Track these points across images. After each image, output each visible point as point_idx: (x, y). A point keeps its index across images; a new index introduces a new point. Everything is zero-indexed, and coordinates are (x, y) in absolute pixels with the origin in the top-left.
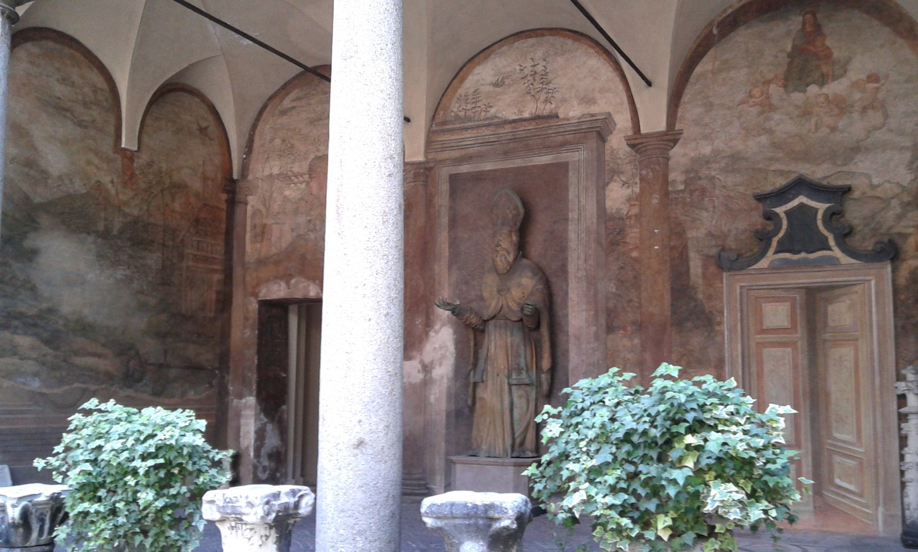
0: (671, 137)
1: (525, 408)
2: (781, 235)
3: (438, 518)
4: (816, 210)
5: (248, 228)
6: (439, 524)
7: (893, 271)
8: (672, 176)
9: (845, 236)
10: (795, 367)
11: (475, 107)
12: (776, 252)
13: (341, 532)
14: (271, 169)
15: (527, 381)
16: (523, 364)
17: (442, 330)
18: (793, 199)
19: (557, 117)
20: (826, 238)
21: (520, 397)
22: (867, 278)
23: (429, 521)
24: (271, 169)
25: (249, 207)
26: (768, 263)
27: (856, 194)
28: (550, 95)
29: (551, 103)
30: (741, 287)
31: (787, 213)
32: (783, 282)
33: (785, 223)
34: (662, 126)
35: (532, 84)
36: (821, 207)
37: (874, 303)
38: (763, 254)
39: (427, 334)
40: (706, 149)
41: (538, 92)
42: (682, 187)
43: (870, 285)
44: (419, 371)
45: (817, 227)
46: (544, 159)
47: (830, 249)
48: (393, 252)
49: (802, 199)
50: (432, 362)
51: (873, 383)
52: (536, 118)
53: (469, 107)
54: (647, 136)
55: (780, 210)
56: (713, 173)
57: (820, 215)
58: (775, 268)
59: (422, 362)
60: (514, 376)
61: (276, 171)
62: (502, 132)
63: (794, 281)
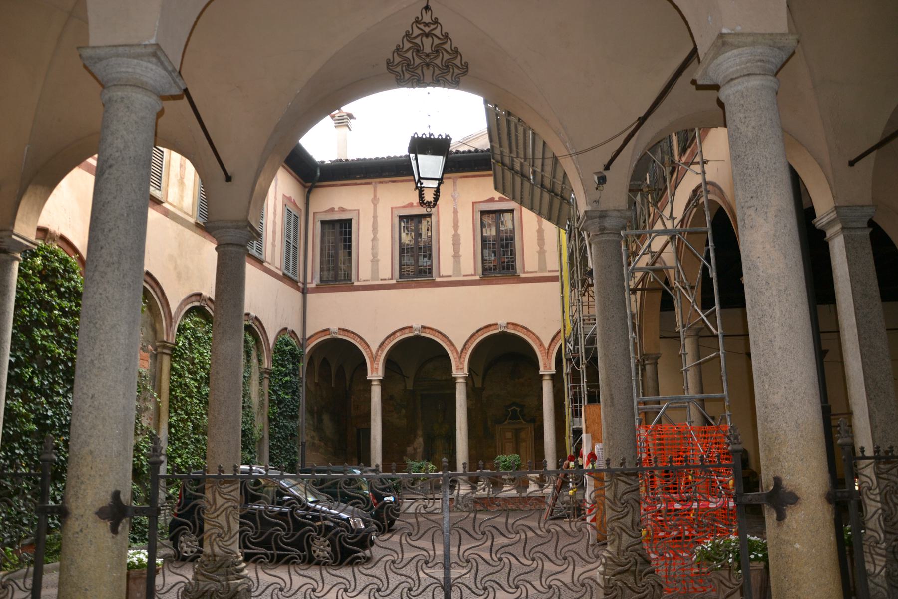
0: (483, 389)
36: (518, 409)
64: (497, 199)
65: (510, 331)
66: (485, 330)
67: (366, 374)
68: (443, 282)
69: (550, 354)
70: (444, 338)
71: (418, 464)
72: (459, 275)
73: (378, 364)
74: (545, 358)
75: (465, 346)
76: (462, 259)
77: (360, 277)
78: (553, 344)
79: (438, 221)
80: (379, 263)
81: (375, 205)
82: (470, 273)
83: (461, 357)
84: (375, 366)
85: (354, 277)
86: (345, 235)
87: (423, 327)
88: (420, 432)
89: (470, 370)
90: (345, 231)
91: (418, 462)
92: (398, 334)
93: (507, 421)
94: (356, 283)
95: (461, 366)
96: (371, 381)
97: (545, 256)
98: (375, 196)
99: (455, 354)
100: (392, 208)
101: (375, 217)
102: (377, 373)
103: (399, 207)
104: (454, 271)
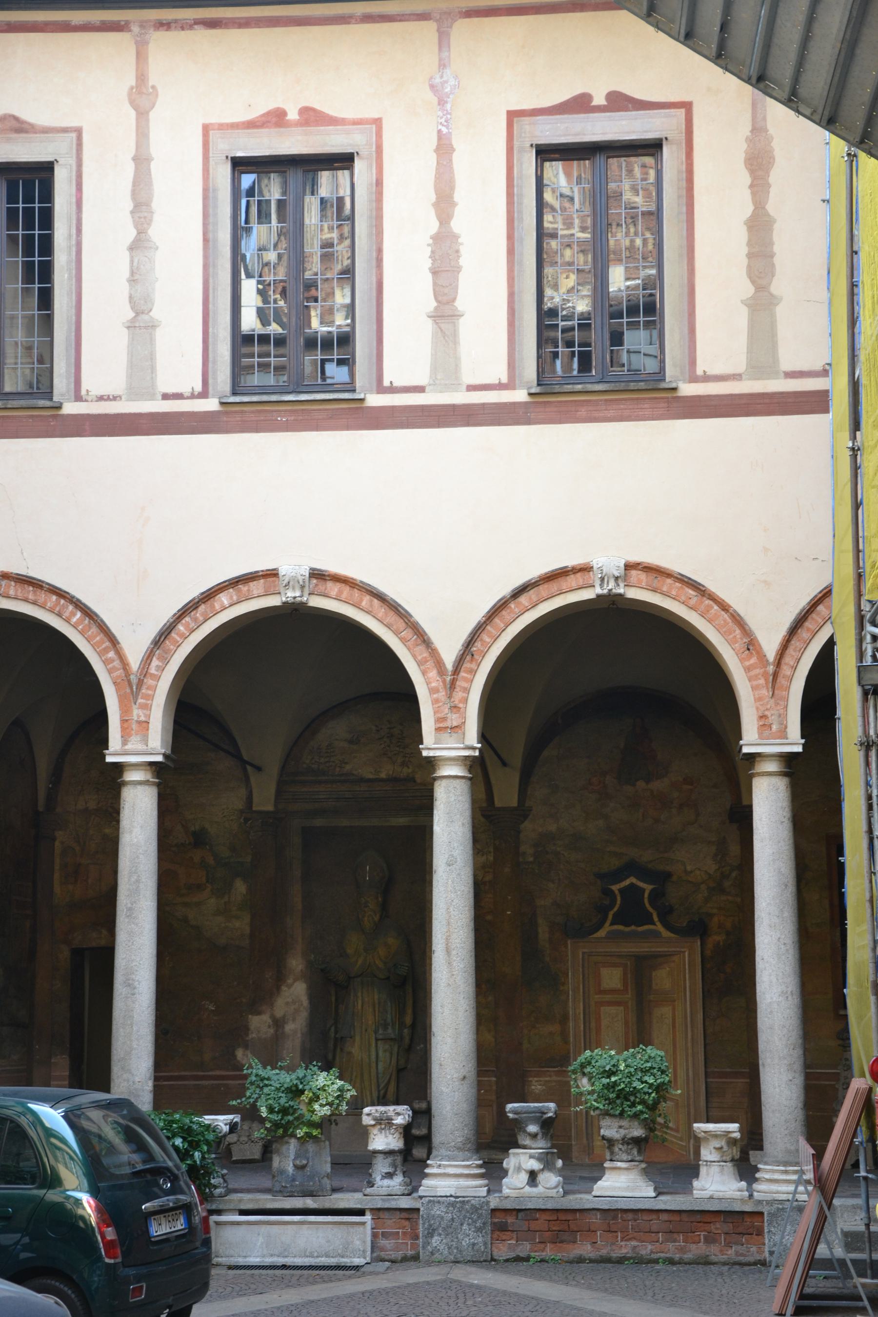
0: (522, 812)
1: (388, 1061)
2: (615, 909)
3: (515, 1114)
4: (644, 890)
5: (57, 867)
6: (516, 1116)
7: (702, 945)
8: (523, 848)
9: (665, 914)
10: (626, 1023)
11: (329, 762)
12: (612, 924)
13: (456, 1125)
14: (86, 803)
15: (392, 1036)
16: (389, 1020)
17: (295, 984)
18: (625, 879)
19: (415, 781)
20: (651, 914)
21: (385, 1051)
22: (683, 950)
23: (511, 1115)
24: (86, 803)
25: (57, 843)
26: (605, 933)
27: (674, 878)
28: (407, 759)
29: (408, 768)
30: (584, 953)
31: (620, 891)
32: (618, 950)
33: (619, 898)
34: (514, 803)
35: (389, 746)
36: (648, 888)
37: (687, 971)
38: (599, 926)
39: (278, 989)
40: (553, 827)
41: (395, 754)
42: (531, 859)
43: (684, 956)
44: (269, 1027)
45: (644, 904)
46: (402, 821)
47: (654, 924)
48: (797, 1075)
49: (632, 880)
50: (284, 1016)
51: (686, 1037)
52: (393, 780)
53: (322, 760)
54: (499, 809)
55: (615, 888)
56: (558, 849)
57: (646, 895)
58: (612, 937)
59: (273, 1017)
60: (381, 1032)
61: (92, 805)
62: (358, 789)
63: (626, 950)
64: (599, 100)
65: (633, 594)
66: (544, 590)
67: (104, 742)
68: (392, 409)
69: (781, 681)
70: (392, 617)
71: (287, 1079)
72: (452, 386)
73: (147, 707)
74: (765, 692)
75: (469, 644)
76: (465, 327)
77: (86, 384)
78: (795, 643)
79: (379, 183)
80: (159, 333)
81: (142, 115)
82: (494, 381)
83: (453, 684)
84: (137, 713)
85: (61, 384)
86: (28, 225)
87: (317, 575)
88: (296, 963)
89: (483, 737)
90: (29, 212)
91: (290, 1069)
92: (223, 598)
93: (607, 928)
94: (70, 408)
95: (454, 719)
96: (119, 768)
97: (773, 316)
98: (141, 77)
99: (433, 674)
100: (206, 129)
101: (142, 161)
102: (145, 740)
103: (234, 126)
104: (434, 369)
